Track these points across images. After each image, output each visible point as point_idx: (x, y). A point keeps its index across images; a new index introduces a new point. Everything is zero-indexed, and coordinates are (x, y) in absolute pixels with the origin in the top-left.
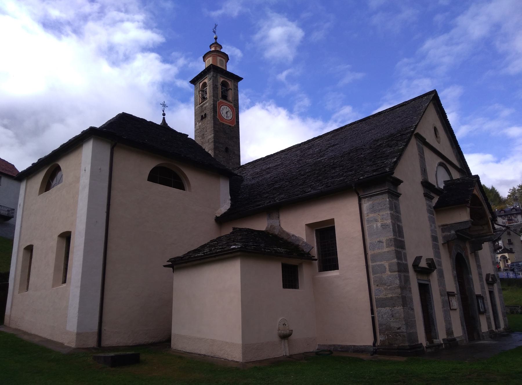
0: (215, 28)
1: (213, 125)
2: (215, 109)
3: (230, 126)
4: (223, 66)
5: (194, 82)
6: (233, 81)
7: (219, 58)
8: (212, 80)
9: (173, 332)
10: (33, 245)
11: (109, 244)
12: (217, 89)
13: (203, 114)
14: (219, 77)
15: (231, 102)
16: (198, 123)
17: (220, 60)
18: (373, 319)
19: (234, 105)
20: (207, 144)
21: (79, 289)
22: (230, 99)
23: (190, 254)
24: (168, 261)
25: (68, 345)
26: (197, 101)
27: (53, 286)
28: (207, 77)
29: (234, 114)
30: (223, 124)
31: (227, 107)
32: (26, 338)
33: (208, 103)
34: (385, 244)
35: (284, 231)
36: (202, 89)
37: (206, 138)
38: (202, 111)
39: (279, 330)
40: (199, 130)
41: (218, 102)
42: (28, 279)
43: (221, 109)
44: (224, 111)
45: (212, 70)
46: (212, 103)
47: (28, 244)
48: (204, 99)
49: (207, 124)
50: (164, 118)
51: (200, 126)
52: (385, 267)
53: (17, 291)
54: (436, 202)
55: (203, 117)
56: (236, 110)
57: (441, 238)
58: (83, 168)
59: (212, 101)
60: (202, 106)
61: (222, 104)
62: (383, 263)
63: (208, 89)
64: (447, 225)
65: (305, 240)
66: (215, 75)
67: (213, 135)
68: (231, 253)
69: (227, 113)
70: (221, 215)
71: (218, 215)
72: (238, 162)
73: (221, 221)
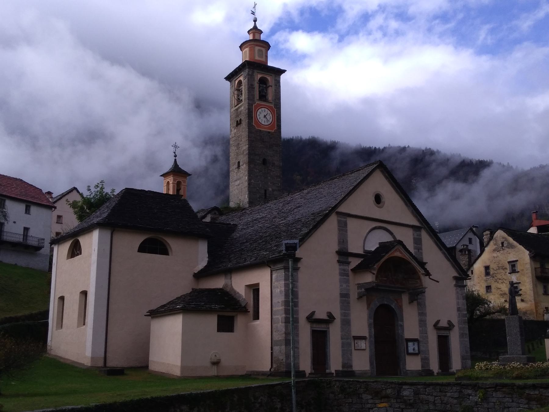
0: (254, 7)
1: (248, 134)
2: (250, 115)
3: (269, 132)
4: (262, 57)
5: (229, 78)
6: (273, 75)
7: (257, 48)
8: (247, 79)
9: (150, 359)
10: (64, 297)
11: (111, 300)
12: (253, 89)
13: (239, 119)
14: (255, 74)
15: (271, 103)
16: (233, 129)
17: (259, 50)
18: (272, 353)
19: (275, 105)
20: (242, 156)
21: (92, 330)
22: (270, 99)
23: (159, 309)
24: (147, 312)
25: (87, 365)
26: (233, 102)
27: (78, 327)
28: (242, 75)
29: (275, 117)
30: (260, 130)
31: (266, 109)
32: (62, 360)
33: (243, 107)
34: (280, 304)
35: (233, 289)
36: (238, 88)
37: (241, 148)
38: (237, 116)
39: (211, 359)
40: (234, 138)
41: (254, 105)
42: (62, 322)
43: (258, 113)
44: (262, 116)
45: (247, 67)
46: (247, 107)
47: (61, 295)
48: (239, 101)
49: (242, 132)
50: (175, 160)
51: (235, 134)
52: (279, 319)
53: (55, 328)
54: (357, 264)
55: (239, 123)
56: (278, 111)
57: (357, 294)
58: (93, 249)
59: (247, 104)
60: (237, 110)
61: (259, 107)
62: (278, 317)
63: (244, 88)
64: (360, 284)
65: (244, 297)
66: (250, 73)
67: (247, 146)
68: (177, 310)
69: (265, 116)
70: (198, 272)
71: (196, 272)
72: (279, 175)
73: (199, 276)
